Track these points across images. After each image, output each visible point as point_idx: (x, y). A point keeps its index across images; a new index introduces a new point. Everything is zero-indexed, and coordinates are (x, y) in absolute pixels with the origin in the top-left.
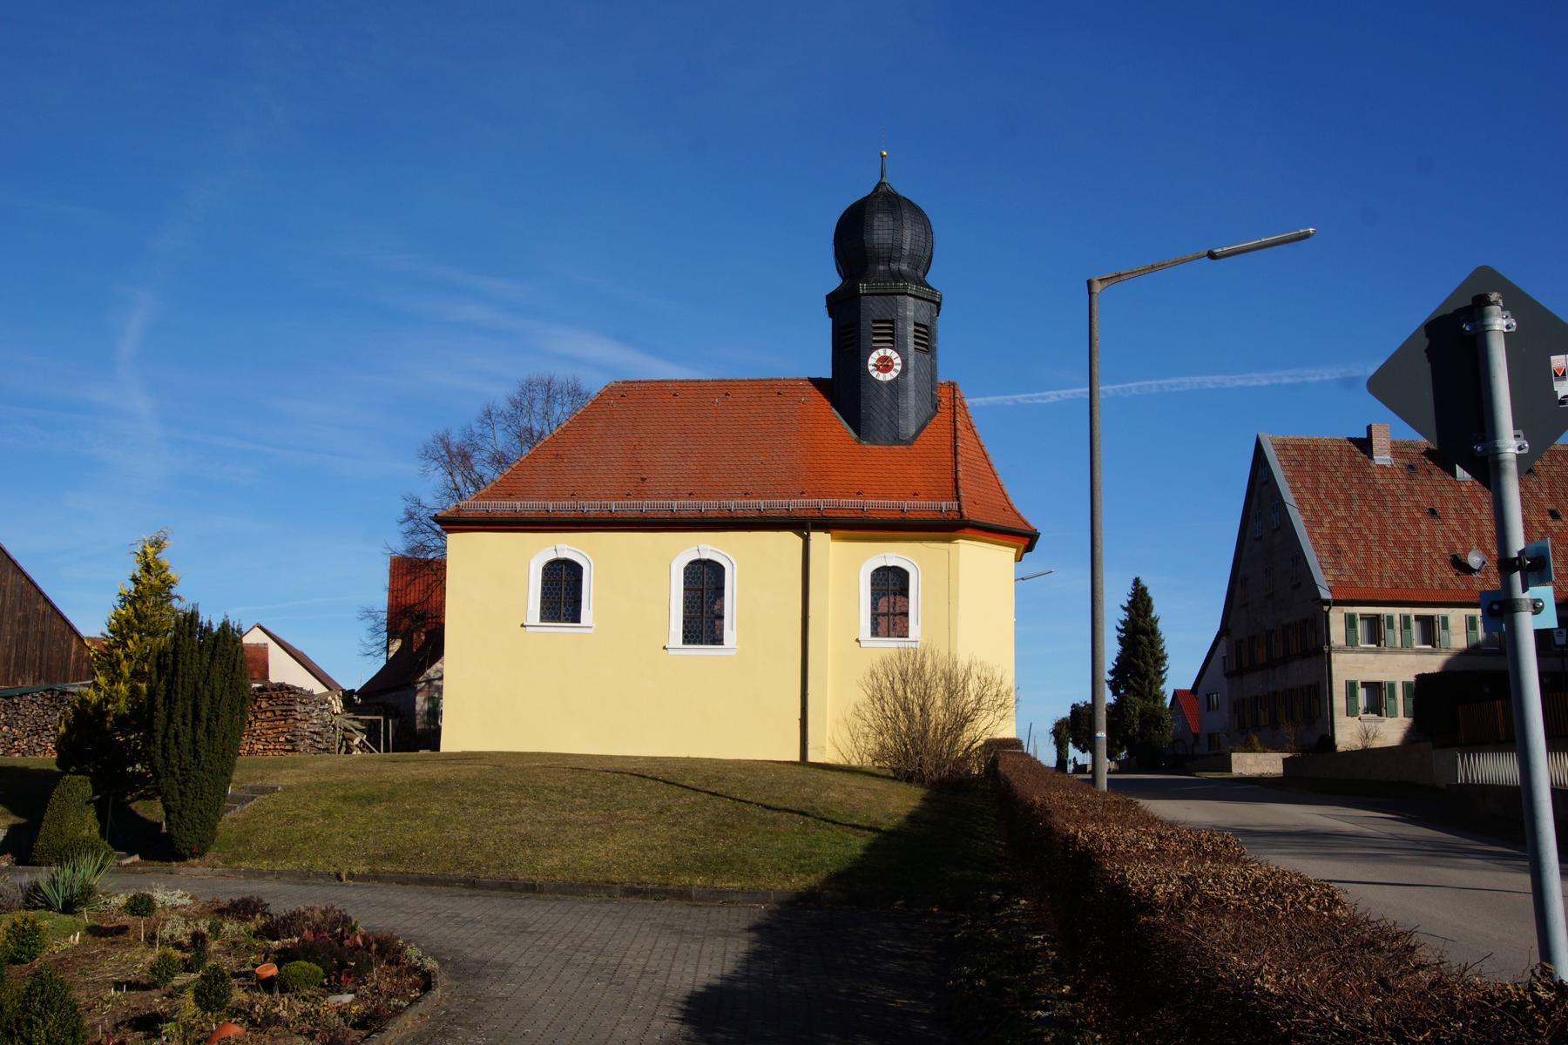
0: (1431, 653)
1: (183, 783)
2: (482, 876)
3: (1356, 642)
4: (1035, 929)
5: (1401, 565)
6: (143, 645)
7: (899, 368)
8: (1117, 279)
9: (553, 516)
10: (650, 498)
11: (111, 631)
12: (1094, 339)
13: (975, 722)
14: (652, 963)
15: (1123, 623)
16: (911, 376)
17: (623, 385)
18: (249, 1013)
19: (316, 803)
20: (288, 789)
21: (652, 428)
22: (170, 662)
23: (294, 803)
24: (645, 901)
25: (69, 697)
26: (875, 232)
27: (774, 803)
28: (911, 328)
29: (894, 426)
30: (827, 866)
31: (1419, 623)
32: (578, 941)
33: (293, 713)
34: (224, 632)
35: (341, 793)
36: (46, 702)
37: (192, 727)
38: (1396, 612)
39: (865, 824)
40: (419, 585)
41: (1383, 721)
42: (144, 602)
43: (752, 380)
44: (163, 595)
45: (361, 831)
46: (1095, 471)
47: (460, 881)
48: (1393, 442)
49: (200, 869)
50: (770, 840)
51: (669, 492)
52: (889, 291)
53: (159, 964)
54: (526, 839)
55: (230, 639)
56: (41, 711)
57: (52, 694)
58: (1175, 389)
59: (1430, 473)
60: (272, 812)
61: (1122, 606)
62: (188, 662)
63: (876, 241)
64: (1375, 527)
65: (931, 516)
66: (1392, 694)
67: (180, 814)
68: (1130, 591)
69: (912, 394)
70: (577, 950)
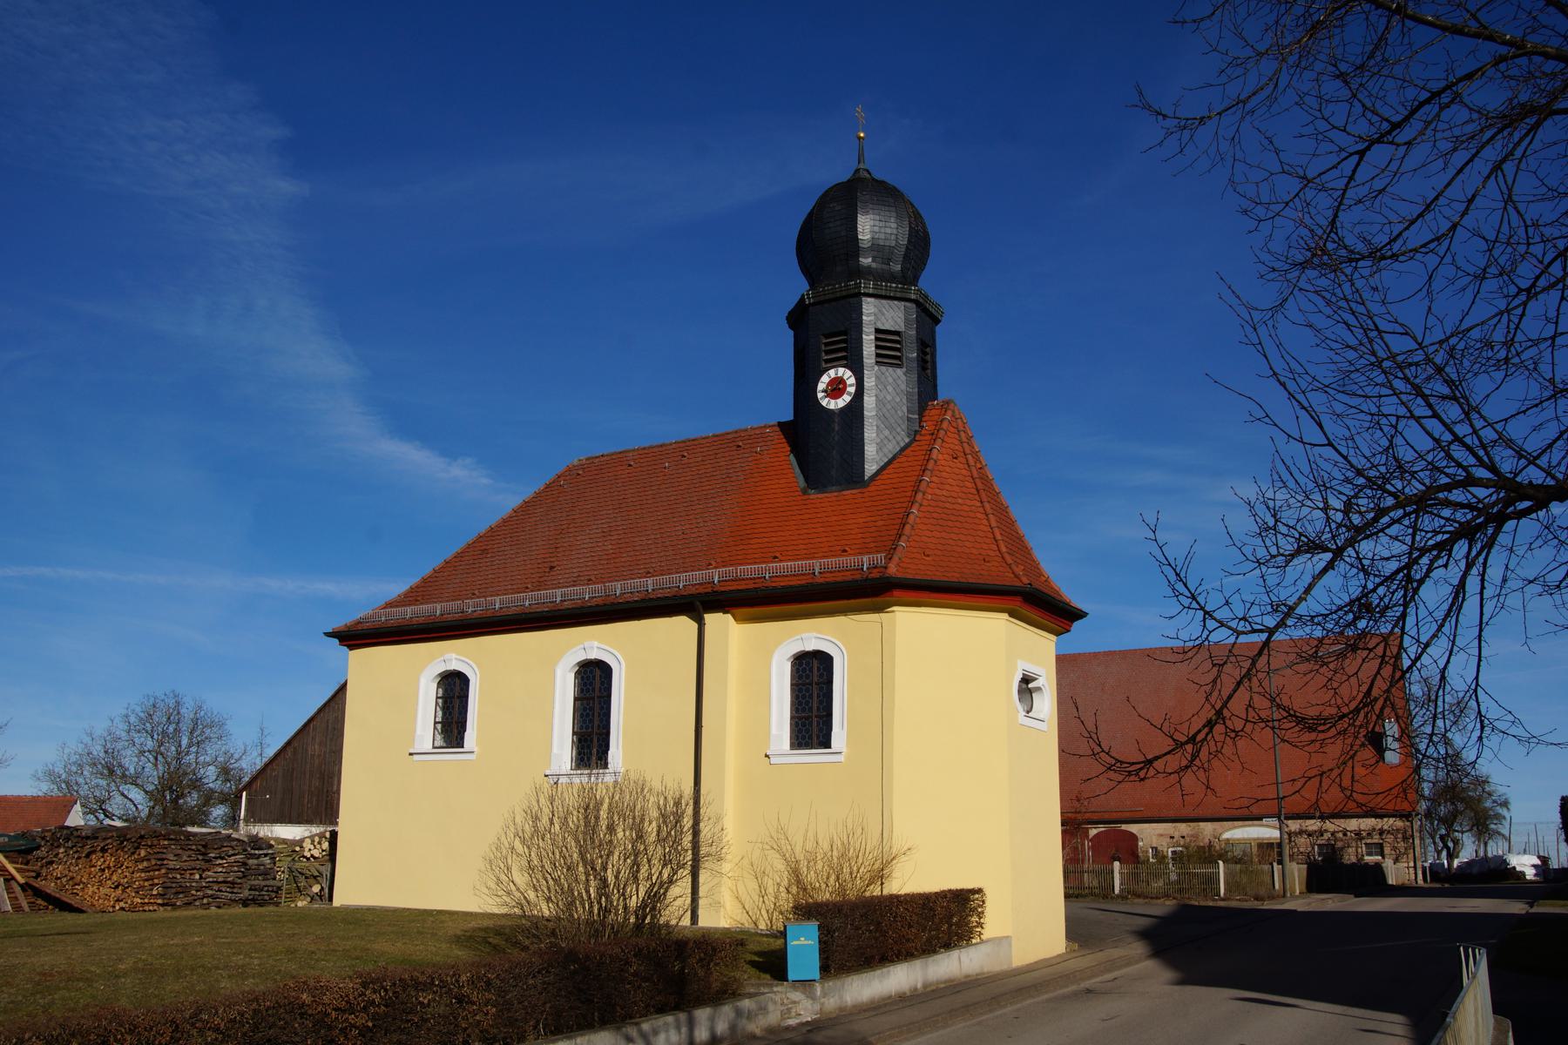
7: (852, 390)
33: (165, 862)
52: (838, 295)
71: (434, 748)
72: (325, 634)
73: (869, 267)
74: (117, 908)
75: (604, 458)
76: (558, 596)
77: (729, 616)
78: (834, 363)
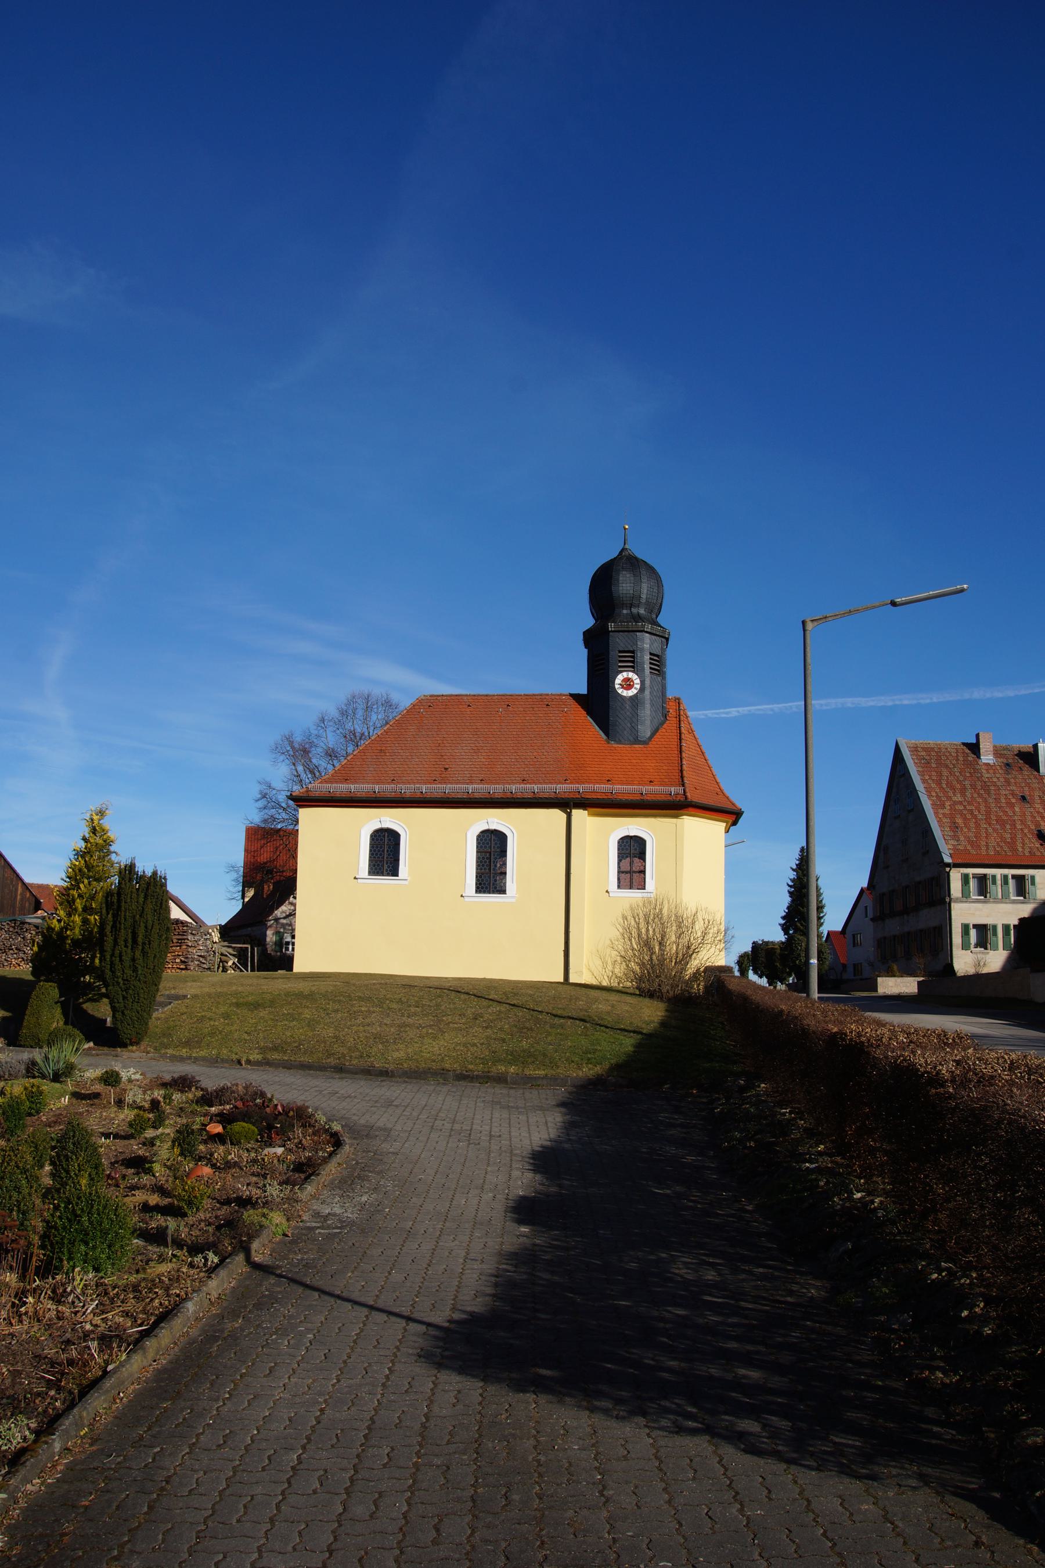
0: (1023, 903)
1: (125, 990)
2: (347, 1064)
3: (969, 895)
4: (782, 1104)
5: (1002, 837)
6: (91, 888)
7: (638, 686)
8: (824, 620)
9: (378, 796)
10: (451, 783)
11: (68, 877)
12: (807, 664)
13: (700, 953)
14: (494, 1129)
15: (793, 880)
16: (647, 692)
17: (430, 698)
18: (210, 1159)
19: (217, 1008)
20: (195, 997)
21: (452, 730)
22: (115, 901)
23: (201, 1007)
24: (473, 1084)
25: (27, 926)
26: (620, 585)
27: (559, 1012)
28: (647, 657)
29: (634, 730)
30: (608, 1059)
31: (1014, 880)
32: (433, 1112)
33: (186, 941)
34: (154, 879)
35: (234, 1001)
36: (11, 929)
37: (132, 949)
38: (998, 872)
39: (630, 1029)
40: (269, 848)
41: (988, 953)
42: (92, 856)
43: (527, 695)
44: (105, 851)
45: (253, 1029)
46: (809, 764)
47: (331, 1067)
48: (995, 747)
49: (137, 1054)
50: (561, 1040)
51: (466, 778)
52: (630, 629)
53: (135, 1120)
54: (377, 1037)
55: (159, 884)
56: (7, 935)
57: (15, 923)
58: (824, 708)
59: (1021, 770)
60: (185, 1013)
61: (791, 868)
62: (129, 900)
63: (621, 592)
64: (983, 808)
65: (663, 798)
66: (995, 934)
67: (123, 1013)
68: (798, 857)
69: (648, 706)
70: (436, 1119)
76: (449, 789)
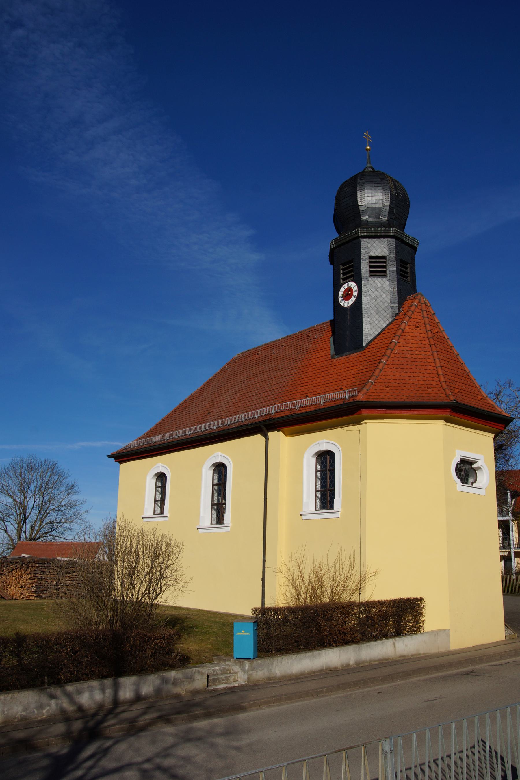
7: (356, 294)
52: (347, 239)
71: (154, 514)
72: (107, 456)
73: (367, 221)
74: (21, 598)
75: (249, 352)
77: (280, 433)
78: (346, 280)
